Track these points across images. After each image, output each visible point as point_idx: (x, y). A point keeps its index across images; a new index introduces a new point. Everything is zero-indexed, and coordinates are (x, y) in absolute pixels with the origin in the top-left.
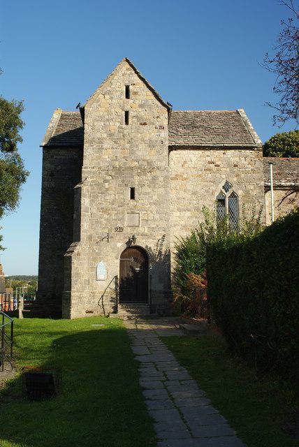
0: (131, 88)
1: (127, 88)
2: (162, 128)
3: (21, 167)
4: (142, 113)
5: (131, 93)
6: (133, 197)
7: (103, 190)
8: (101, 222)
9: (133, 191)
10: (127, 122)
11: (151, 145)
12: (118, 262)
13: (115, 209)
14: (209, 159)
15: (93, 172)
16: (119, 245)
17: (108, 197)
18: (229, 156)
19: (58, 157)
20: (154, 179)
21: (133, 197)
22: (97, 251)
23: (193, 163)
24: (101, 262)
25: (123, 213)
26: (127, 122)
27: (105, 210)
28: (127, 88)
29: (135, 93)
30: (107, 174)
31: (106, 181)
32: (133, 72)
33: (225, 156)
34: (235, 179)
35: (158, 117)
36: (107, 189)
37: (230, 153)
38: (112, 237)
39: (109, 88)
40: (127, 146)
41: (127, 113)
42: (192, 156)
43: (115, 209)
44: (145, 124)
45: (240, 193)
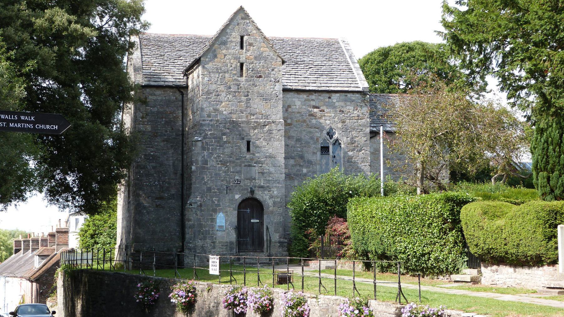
0: (245, 38)
1: (242, 38)
3: (386, 49)
4: (259, 65)
6: (248, 149)
7: (222, 143)
8: (219, 174)
9: (248, 143)
10: (242, 47)
12: (236, 212)
13: (234, 162)
14: (313, 103)
15: (211, 125)
16: (237, 197)
17: (226, 150)
18: (335, 101)
19: (155, 98)
20: (270, 132)
21: (248, 149)
22: (216, 202)
23: (297, 107)
24: (221, 214)
25: (240, 166)
26: (242, 47)
27: (224, 163)
28: (242, 38)
29: (251, 45)
30: (225, 127)
31: (224, 134)
33: (330, 100)
34: (340, 125)
35: (273, 70)
36: (225, 142)
38: (230, 190)
39: (224, 38)
40: (244, 98)
41: (242, 65)
42: (296, 100)
43: (234, 162)
44: (260, 77)
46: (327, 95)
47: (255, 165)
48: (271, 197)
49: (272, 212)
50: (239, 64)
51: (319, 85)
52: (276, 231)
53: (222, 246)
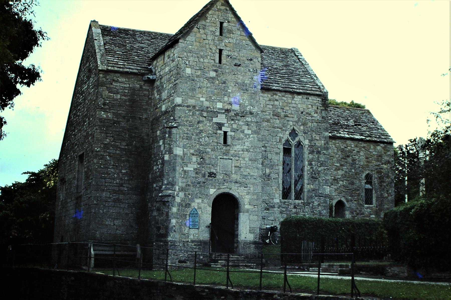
0: (225, 25)
2: (255, 71)
5: (225, 31)
11: (243, 88)
28: (221, 24)
29: (230, 32)
32: (228, 9)
37: (298, 98)
45: (306, 142)
46: (289, 96)
47: (232, 158)
48: (248, 193)
49: (248, 211)
50: (218, 51)
51: (283, 86)
52: (251, 231)
53: (195, 245)
